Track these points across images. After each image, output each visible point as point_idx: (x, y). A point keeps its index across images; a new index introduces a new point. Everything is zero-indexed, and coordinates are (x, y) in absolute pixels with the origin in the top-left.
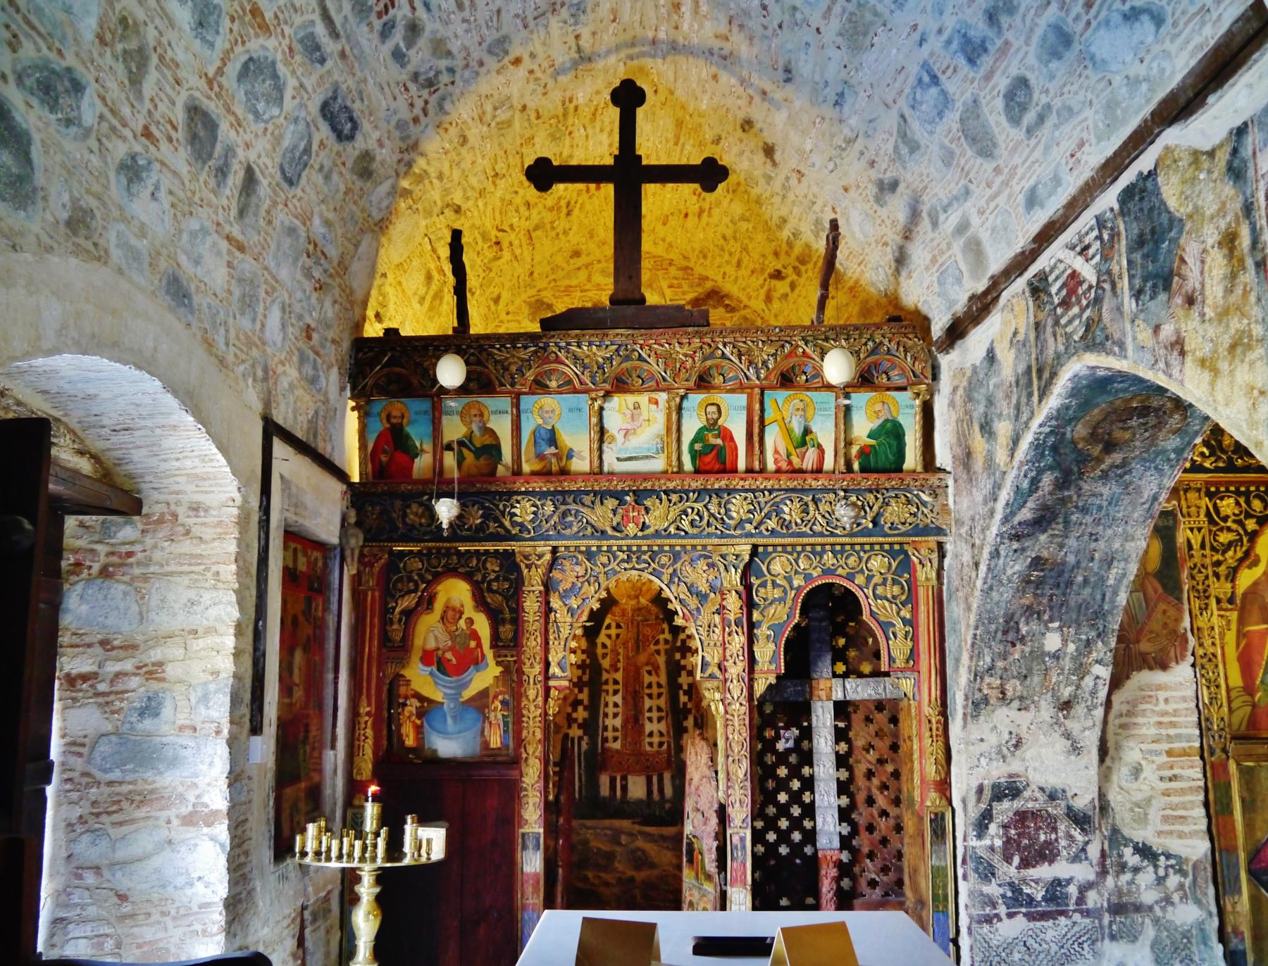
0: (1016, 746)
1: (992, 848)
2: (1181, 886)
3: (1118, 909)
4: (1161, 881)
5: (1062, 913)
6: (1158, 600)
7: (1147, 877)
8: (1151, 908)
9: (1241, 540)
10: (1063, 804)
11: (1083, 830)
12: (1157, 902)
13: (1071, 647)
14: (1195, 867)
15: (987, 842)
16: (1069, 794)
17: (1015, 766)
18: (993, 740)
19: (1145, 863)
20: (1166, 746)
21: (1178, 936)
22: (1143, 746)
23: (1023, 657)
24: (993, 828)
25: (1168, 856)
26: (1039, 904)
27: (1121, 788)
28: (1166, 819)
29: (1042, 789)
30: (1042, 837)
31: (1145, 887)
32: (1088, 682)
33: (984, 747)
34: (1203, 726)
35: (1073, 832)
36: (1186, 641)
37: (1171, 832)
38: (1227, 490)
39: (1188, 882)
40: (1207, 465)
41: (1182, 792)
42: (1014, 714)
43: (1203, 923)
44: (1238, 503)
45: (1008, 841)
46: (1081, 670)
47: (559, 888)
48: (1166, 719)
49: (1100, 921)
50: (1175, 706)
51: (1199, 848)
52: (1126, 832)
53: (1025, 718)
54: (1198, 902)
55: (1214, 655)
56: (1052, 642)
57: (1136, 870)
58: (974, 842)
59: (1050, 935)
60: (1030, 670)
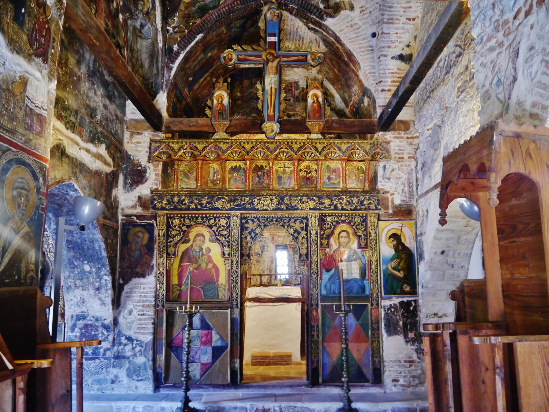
0: (83, 302)
1: (76, 336)
2: (140, 351)
3: (117, 357)
4: (133, 349)
5: (97, 358)
6: (145, 254)
7: (129, 347)
8: (128, 358)
9: (180, 234)
10: (101, 322)
11: (107, 331)
12: (131, 356)
13: (94, 270)
14: (146, 344)
15: (74, 334)
16: (103, 319)
17: (84, 309)
18: (75, 300)
19: (129, 342)
20: (142, 304)
21: (137, 367)
22: (134, 304)
23: (79, 273)
24: (76, 329)
25: (137, 341)
26: (90, 355)
27: (124, 317)
28: (138, 328)
29: (93, 317)
30: (93, 333)
31: (128, 351)
32: (103, 281)
33: (72, 302)
34: (156, 297)
35: (103, 331)
36: (153, 268)
37: (139, 333)
38: (177, 216)
39: (143, 349)
40: (167, 207)
41: (145, 319)
42: (81, 292)
43: (146, 363)
44: (180, 221)
45: (81, 334)
46: (100, 278)
47: (306, 351)
48: (143, 295)
49: (110, 361)
50: (147, 290)
51: (149, 338)
52: (123, 332)
53: (85, 293)
54: (145, 356)
55: (163, 273)
56: (87, 268)
57: (125, 345)
58: (70, 334)
59: (92, 365)
60: (82, 277)
